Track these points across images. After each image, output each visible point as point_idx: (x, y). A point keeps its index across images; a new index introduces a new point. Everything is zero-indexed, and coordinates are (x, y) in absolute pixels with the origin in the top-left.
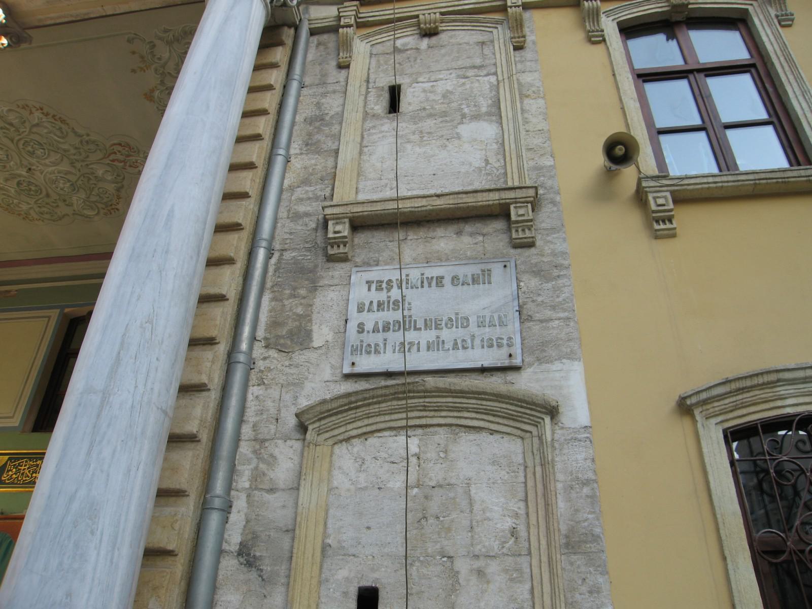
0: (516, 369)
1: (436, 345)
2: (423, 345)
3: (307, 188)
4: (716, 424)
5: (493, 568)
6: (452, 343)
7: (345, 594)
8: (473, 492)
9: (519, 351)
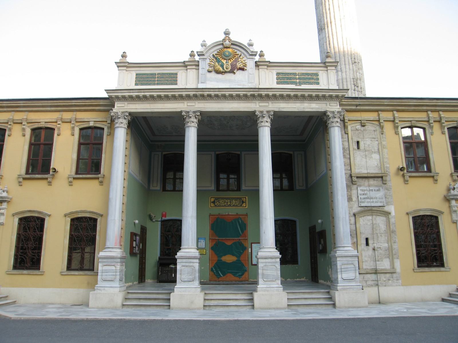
0: (384, 206)
5: (383, 235)
7: (364, 239)
8: (379, 224)
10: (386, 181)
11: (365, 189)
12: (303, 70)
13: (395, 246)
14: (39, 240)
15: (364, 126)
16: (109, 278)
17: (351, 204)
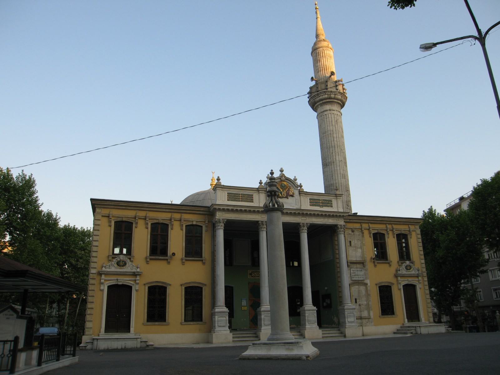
10: (365, 265)
13: (370, 303)
14: (382, 303)
15: (353, 232)
16: (222, 325)
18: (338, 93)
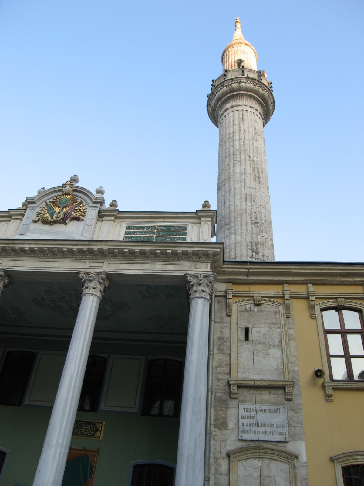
0: (287, 442)
1: (265, 432)
2: (261, 432)
3: (221, 368)
4: (340, 465)
6: (269, 432)
8: (276, 479)
9: (288, 437)
11: (252, 408)
12: (164, 222)
17: (224, 435)
18: (245, 79)
